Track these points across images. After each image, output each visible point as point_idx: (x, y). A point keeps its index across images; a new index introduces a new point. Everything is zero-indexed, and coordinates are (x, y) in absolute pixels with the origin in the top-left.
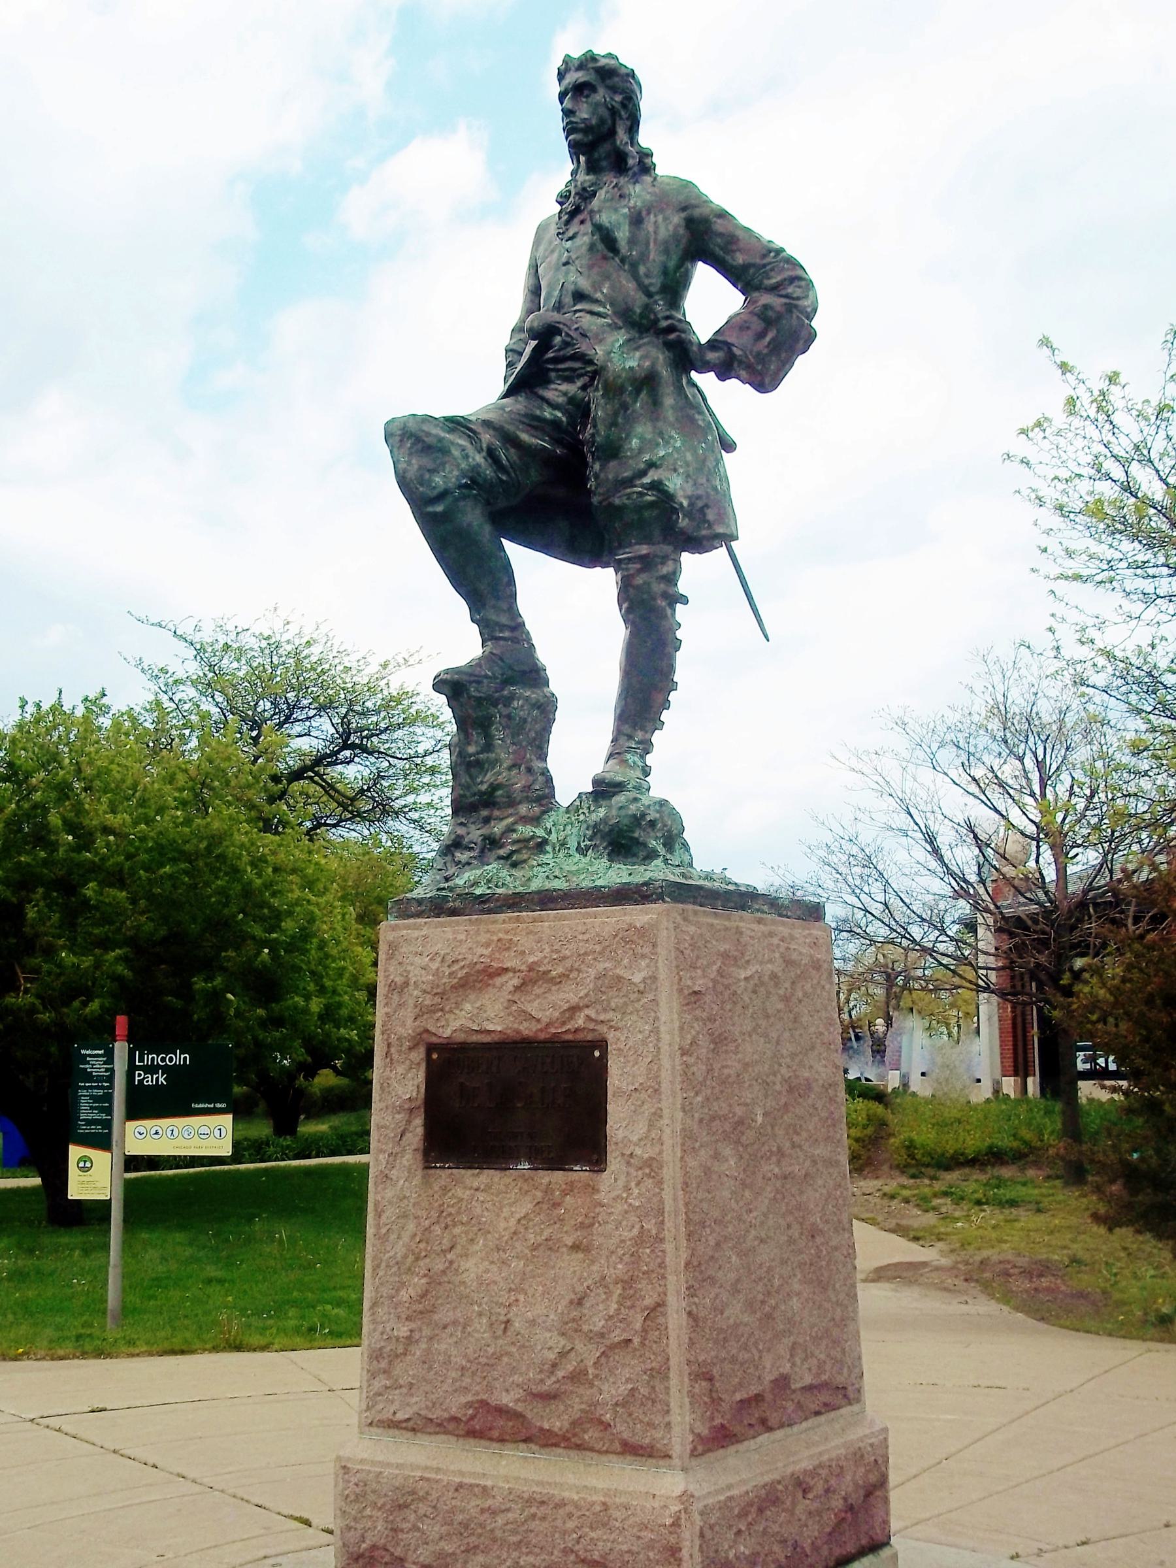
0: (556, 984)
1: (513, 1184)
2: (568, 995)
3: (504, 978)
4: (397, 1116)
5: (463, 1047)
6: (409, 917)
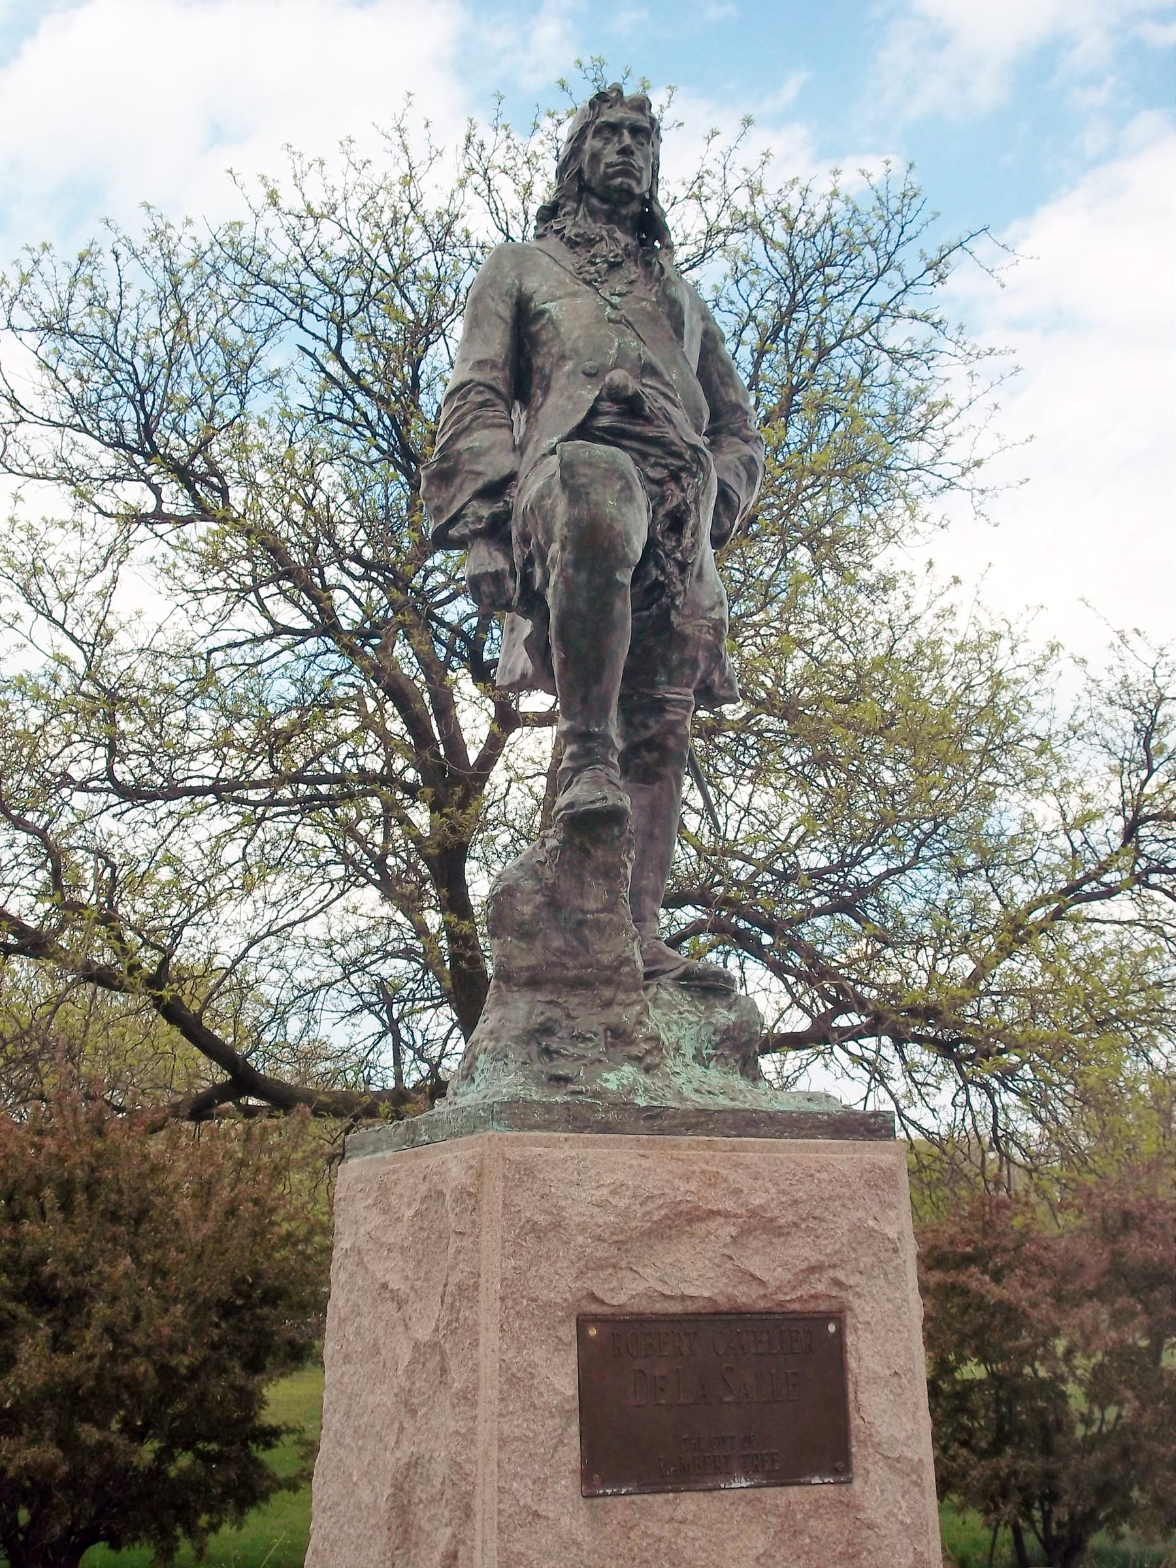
0: (780, 1235)
1: (732, 1510)
2: (802, 1251)
3: (712, 1225)
4: (549, 1422)
5: (638, 1321)
6: (532, 1127)
